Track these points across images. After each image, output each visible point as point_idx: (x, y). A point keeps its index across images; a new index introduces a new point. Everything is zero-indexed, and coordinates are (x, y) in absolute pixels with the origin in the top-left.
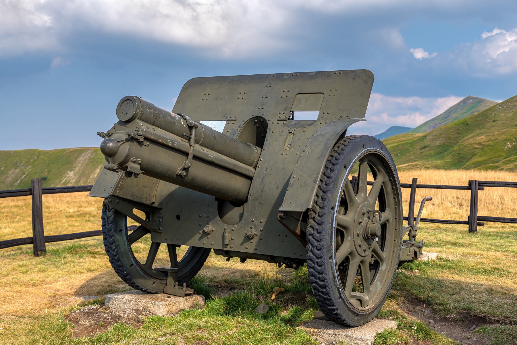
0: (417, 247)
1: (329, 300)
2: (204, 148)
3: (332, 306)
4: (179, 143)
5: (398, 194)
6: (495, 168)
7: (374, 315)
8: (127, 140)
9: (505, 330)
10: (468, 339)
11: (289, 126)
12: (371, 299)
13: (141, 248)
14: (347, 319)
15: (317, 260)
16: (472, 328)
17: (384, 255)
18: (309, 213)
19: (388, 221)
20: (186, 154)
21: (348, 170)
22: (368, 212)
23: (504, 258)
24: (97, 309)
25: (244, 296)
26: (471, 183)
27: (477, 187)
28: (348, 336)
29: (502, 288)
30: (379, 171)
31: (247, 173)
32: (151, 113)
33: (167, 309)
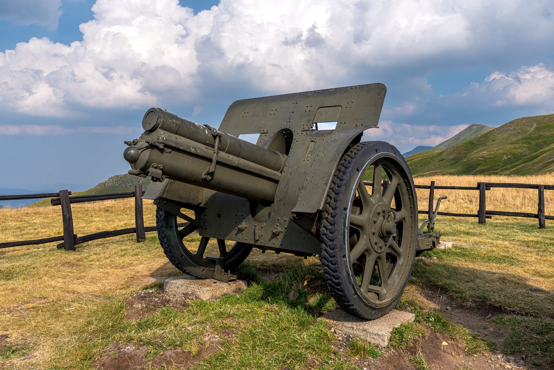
0: (435, 237)
1: (344, 297)
2: (229, 155)
3: (348, 302)
4: (203, 151)
5: (412, 194)
6: (496, 174)
7: (391, 307)
8: (147, 148)
9: (522, 322)
10: (485, 328)
11: (311, 136)
12: (388, 293)
13: (192, 243)
14: (364, 314)
15: (331, 259)
16: (488, 317)
17: (401, 250)
18: (323, 214)
19: (404, 219)
20: (210, 160)
21: (360, 173)
22: (384, 212)
23: (511, 246)
24: (152, 293)
25: (280, 283)
26: (479, 184)
27: (485, 188)
28: (364, 330)
29: (514, 277)
30: (394, 174)
31: (274, 177)
32: (173, 123)
33: (211, 294)
